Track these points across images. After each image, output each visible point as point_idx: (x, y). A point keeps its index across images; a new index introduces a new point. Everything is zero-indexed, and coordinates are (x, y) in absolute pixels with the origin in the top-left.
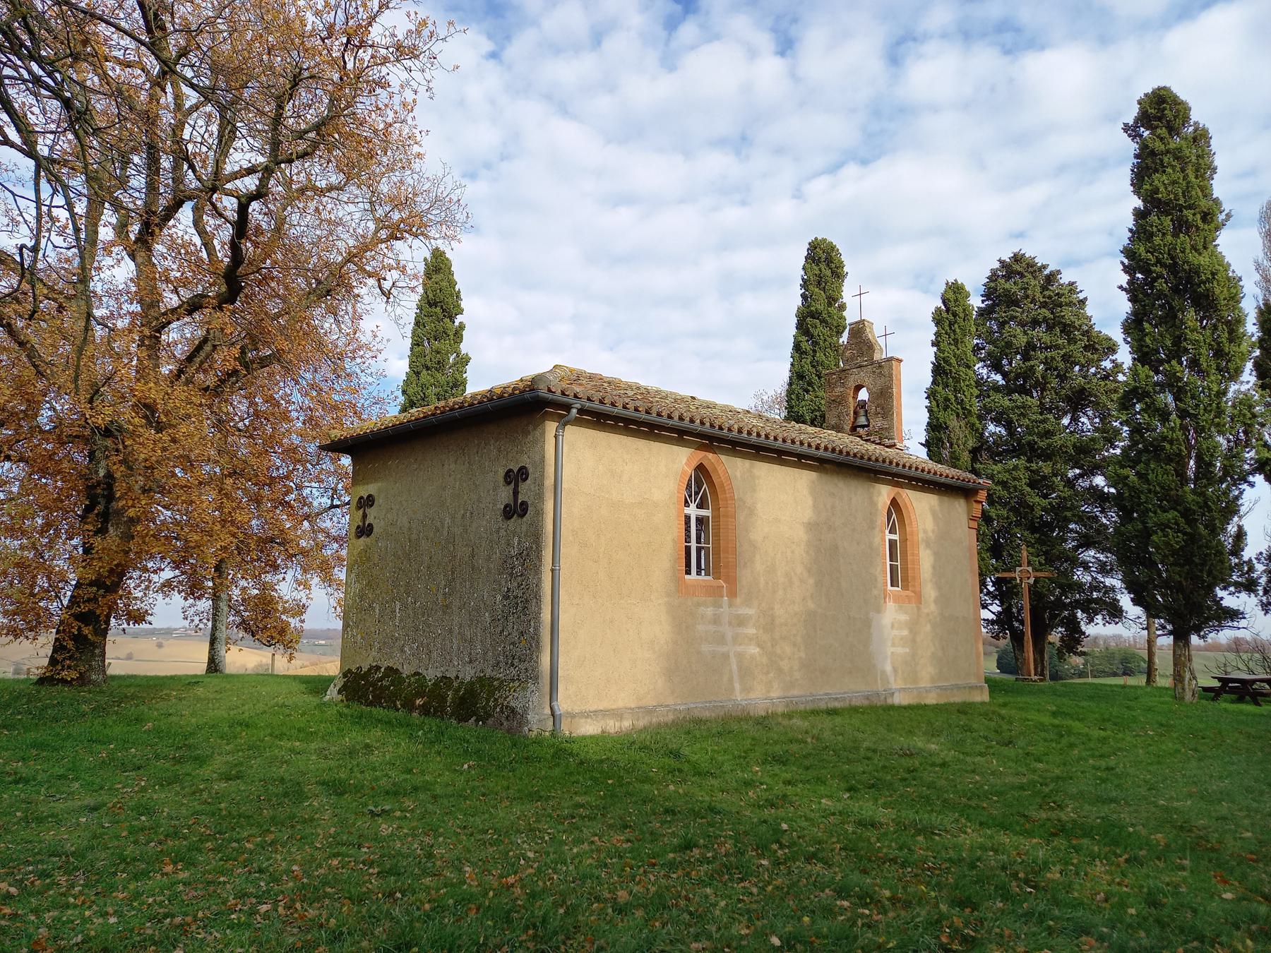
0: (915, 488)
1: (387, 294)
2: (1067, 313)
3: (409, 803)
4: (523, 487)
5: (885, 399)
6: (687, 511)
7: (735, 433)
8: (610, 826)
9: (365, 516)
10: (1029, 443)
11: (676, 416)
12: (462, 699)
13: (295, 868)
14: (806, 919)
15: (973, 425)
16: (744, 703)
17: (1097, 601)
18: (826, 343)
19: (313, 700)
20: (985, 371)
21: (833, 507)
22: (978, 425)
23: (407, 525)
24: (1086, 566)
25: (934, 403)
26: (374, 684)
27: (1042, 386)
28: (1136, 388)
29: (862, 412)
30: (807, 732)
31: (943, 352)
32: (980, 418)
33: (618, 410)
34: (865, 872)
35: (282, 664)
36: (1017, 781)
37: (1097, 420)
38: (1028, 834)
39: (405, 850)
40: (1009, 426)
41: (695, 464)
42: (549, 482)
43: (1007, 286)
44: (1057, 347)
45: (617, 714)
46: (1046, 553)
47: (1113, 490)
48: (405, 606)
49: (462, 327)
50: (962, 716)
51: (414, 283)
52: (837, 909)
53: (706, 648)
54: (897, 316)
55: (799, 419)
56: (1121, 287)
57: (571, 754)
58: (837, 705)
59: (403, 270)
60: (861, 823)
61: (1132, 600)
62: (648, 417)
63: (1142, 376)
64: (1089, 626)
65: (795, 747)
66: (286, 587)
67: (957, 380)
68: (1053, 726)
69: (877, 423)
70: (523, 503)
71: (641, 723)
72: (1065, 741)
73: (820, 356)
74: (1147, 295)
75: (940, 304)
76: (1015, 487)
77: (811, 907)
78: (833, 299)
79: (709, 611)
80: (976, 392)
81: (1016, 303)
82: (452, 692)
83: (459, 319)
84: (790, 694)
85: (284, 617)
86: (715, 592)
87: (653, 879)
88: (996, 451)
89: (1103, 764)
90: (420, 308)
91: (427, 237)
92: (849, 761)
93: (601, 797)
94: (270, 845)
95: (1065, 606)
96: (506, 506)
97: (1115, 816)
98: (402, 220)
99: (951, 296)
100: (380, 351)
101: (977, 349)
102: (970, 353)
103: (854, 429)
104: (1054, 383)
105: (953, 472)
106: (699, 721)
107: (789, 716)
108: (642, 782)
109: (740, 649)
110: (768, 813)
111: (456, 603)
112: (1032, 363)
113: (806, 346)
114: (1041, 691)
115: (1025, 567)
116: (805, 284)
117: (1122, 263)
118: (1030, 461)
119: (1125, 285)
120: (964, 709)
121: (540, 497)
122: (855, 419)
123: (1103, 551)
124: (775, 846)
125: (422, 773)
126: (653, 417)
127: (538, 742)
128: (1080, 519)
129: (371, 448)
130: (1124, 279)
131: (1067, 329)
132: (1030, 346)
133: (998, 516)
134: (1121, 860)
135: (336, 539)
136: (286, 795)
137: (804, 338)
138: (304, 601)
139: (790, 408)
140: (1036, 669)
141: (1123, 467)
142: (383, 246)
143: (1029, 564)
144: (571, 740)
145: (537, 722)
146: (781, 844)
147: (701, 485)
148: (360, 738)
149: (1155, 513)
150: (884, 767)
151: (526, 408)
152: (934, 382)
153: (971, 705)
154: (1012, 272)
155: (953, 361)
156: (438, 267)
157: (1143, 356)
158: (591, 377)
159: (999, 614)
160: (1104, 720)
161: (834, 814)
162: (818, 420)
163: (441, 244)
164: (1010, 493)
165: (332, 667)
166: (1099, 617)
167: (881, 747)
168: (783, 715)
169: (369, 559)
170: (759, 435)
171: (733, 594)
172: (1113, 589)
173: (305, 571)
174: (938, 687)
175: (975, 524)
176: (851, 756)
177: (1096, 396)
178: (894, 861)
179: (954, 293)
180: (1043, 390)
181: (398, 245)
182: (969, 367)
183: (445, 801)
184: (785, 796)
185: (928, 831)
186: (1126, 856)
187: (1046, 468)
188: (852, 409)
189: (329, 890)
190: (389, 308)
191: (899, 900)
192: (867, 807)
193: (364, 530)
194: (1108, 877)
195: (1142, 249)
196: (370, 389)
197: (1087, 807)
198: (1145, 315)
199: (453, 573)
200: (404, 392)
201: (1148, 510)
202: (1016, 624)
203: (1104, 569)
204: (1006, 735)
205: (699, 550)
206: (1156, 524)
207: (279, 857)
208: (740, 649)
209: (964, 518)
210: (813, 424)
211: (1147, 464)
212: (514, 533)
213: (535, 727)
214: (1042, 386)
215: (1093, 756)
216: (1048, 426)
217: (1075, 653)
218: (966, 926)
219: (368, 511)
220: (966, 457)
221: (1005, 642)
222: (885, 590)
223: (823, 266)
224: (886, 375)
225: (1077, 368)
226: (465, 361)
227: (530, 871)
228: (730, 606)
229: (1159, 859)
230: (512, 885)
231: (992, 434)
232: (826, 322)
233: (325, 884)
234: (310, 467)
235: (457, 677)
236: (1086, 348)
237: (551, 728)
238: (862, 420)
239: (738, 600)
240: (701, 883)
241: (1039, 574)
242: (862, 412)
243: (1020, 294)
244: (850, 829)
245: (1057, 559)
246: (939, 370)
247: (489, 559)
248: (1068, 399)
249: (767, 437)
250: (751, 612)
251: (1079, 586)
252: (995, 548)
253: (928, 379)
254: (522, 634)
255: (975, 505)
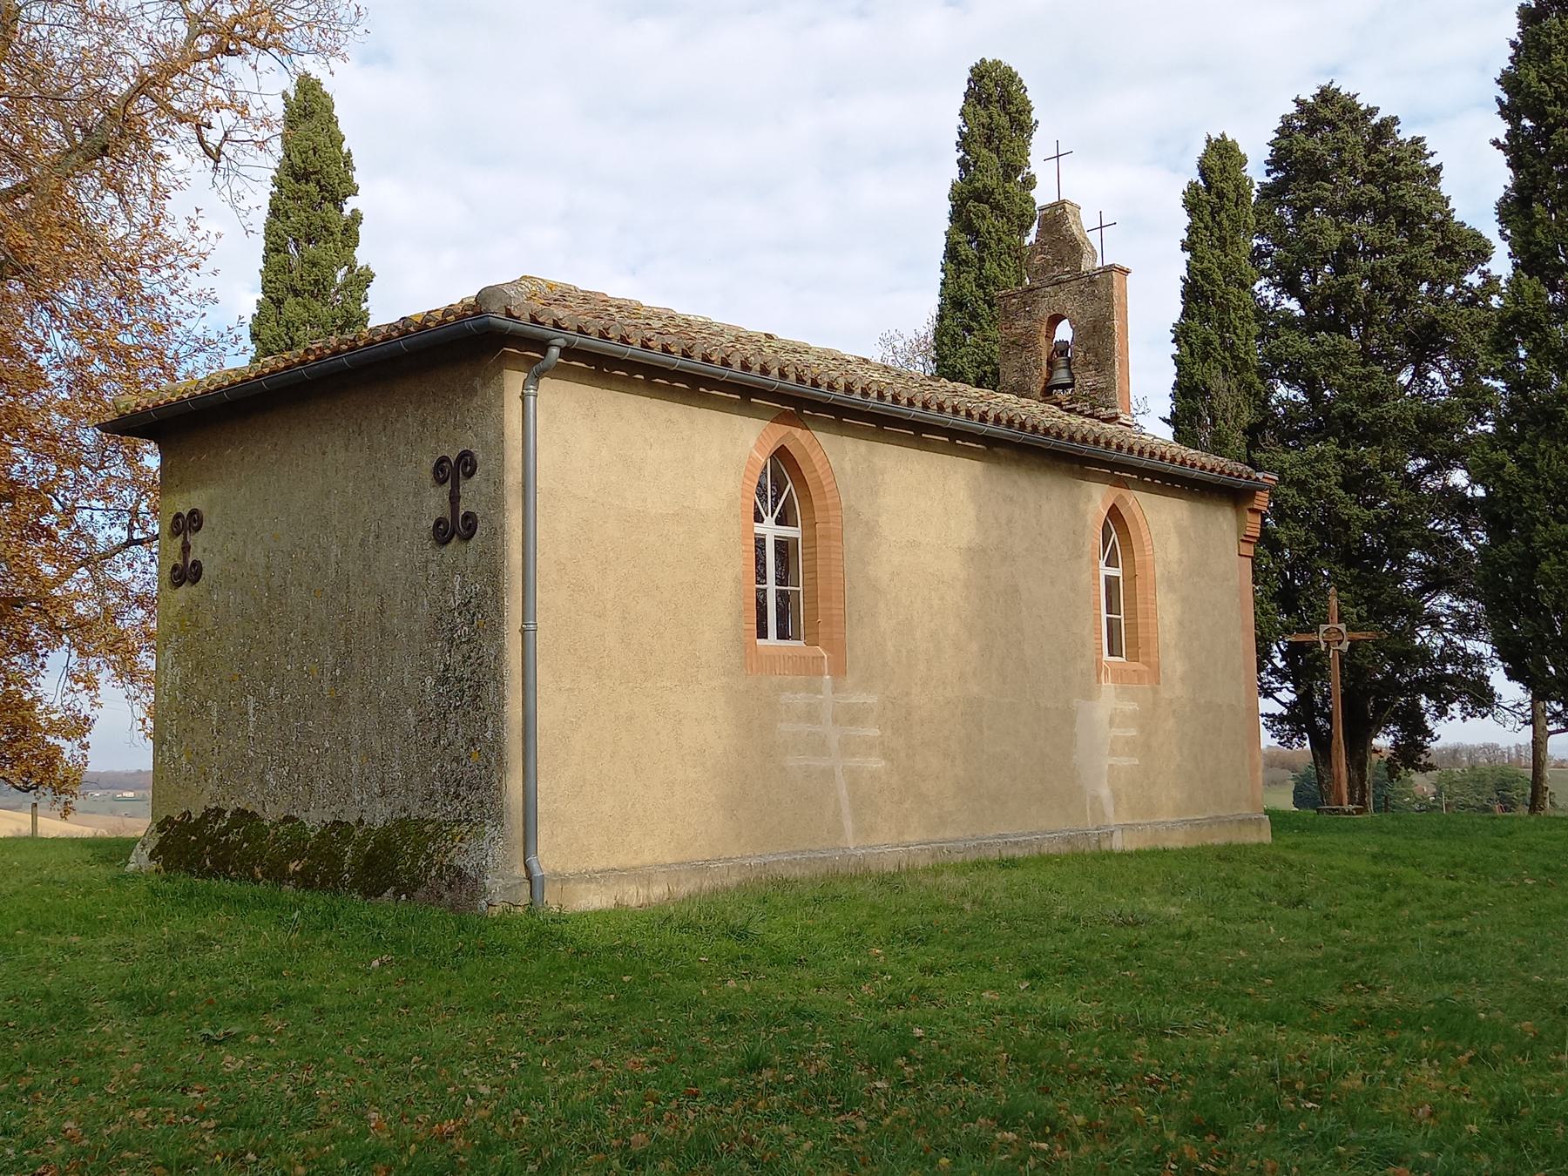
0: (1148, 488)
1: (214, 154)
2: (1409, 194)
3: (274, 1022)
4: (467, 487)
5: (1101, 338)
6: (759, 528)
7: (840, 392)
8: (626, 1044)
9: (186, 548)
10: (1343, 415)
11: (736, 361)
12: (371, 860)
13: (69, 1125)
14: (944, 1161)
15: (1251, 385)
16: (859, 853)
17: (1451, 679)
18: (1004, 248)
19: (102, 872)
20: (1271, 293)
21: (1010, 521)
22: (1258, 385)
23: (263, 561)
24: (1434, 621)
25: (1186, 348)
26: (212, 840)
27: (1366, 316)
28: (1516, 318)
29: (1061, 362)
30: (964, 894)
31: (1201, 260)
32: (1263, 374)
33: (633, 351)
34: (1046, 1091)
35: (52, 826)
36: (1307, 955)
37: (1457, 375)
38: (1316, 1028)
39: (265, 1091)
40: (1311, 388)
41: (771, 447)
42: (513, 478)
43: (1309, 145)
44: (1391, 250)
45: (643, 875)
46: (1369, 600)
47: (1480, 492)
48: (264, 704)
49: (356, 218)
50: (1223, 865)
51: (263, 134)
52: (996, 1144)
53: (792, 761)
54: (1125, 204)
55: (956, 376)
56: (1496, 143)
57: (561, 939)
58: (1019, 853)
59: (243, 111)
60: (1046, 1024)
61: (1507, 671)
62: (686, 363)
63: (1528, 293)
64: (1440, 722)
65: (943, 917)
66: (52, 682)
67: (1224, 308)
68: (1373, 876)
69: (1087, 380)
70: (468, 516)
71: (683, 890)
72: (1390, 896)
73: (991, 268)
74: (1539, 155)
75: (1195, 176)
76: (1319, 490)
77: (953, 1144)
78: (1013, 168)
79: (801, 699)
80: (1255, 329)
81: (1324, 175)
82: (345, 844)
83: (350, 204)
84: (938, 837)
85: (50, 739)
86: (810, 668)
87: (691, 1115)
88: (1289, 430)
89: (1449, 927)
90: (278, 183)
91: (284, 50)
92: (1033, 936)
93: (611, 1004)
94: (26, 1093)
95: (1401, 690)
96: (438, 522)
97: (1459, 998)
98: (238, 19)
99: (1214, 162)
100: (203, 256)
101: (1258, 255)
102: (1246, 263)
103: (1048, 391)
104: (1386, 312)
105: (1211, 460)
106: (782, 884)
107: (937, 871)
108: (682, 978)
109: (854, 762)
110: (893, 1015)
111: (356, 694)
112: (1349, 277)
113: (968, 251)
114: (1359, 828)
115: (1335, 624)
116: (964, 142)
117: (1499, 100)
118: (1343, 444)
119: (1503, 140)
120: (1226, 854)
121: (498, 503)
122: (1050, 374)
123: (1464, 595)
124: (900, 1061)
125: (299, 976)
126: (696, 363)
127: (504, 922)
128: (1428, 543)
129: (192, 425)
130: (1501, 129)
131: (1408, 219)
132: (1347, 249)
133: (1291, 539)
134: (1464, 1058)
135: (140, 602)
136: (54, 1018)
137: (963, 237)
138: (86, 710)
139: (940, 360)
140: (1351, 795)
141: (1494, 448)
142: (204, 65)
143: (1341, 618)
144: (561, 919)
145: (502, 888)
146: (908, 1056)
147: (783, 482)
148: (188, 927)
149: (1546, 524)
150: (1090, 942)
151: (473, 346)
152: (1185, 314)
153: (1243, 849)
154: (1317, 121)
155: (1218, 276)
156: (309, 109)
157: (1530, 259)
158: (586, 298)
159: (1291, 706)
160: (1456, 865)
161: (1001, 1012)
162: (989, 379)
163: (313, 66)
164: (1311, 500)
165: (139, 825)
166: (1456, 706)
167: (1087, 913)
168: (926, 870)
169: (195, 625)
170: (881, 396)
171: (839, 669)
172: (1478, 659)
173: (82, 653)
174: (1191, 822)
175: (1249, 550)
176: (1034, 928)
177: (1455, 333)
178: (1095, 1074)
179: (1221, 158)
180: (1367, 324)
181: (232, 64)
182: (1243, 286)
183: (339, 1017)
184: (922, 988)
185: (1157, 1031)
186: (1471, 1053)
187: (1370, 456)
188: (1045, 357)
189: (127, 1154)
190: (219, 179)
191: (1098, 1128)
192: (1057, 1000)
193: (185, 574)
194: (1439, 1084)
195: (1533, 74)
196: (189, 324)
197: (1415, 987)
198: (1535, 189)
199: (347, 642)
200: (255, 336)
201: (1535, 520)
202: (1320, 722)
203: (1465, 627)
204: (1295, 891)
205: (781, 595)
206: (1547, 543)
207: (40, 1111)
208: (854, 762)
209: (1232, 539)
210: (978, 384)
211: (1534, 443)
212: (454, 568)
213: (498, 899)
214: (1366, 316)
215: (1433, 917)
216: (1375, 385)
217: (1416, 767)
218: (1203, 1160)
219: (191, 539)
220: (1238, 440)
221: (1304, 748)
222: (1099, 662)
223: (996, 110)
224: (1099, 294)
225: (1424, 287)
226: (363, 280)
227: (483, 1113)
228: (835, 690)
229: (1522, 1053)
230: (451, 1135)
231: (1281, 402)
232: (1002, 210)
233: (120, 1147)
234: (87, 472)
235: (361, 821)
236: (1439, 251)
237: (526, 900)
238: (1062, 376)
239: (849, 680)
240: (773, 1118)
241: (1357, 635)
242: (1061, 362)
243: (1331, 159)
244: (1027, 1033)
245: (1388, 609)
246: (1193, 292)
247: (410, 615)
248: (1410, 340)
249: (895, 399)
250: (872, 699)
251: (1424, 654)
252: (1283, 596)
253: (1174, 309)
254: (472, 742)
255: (1250, 516)
